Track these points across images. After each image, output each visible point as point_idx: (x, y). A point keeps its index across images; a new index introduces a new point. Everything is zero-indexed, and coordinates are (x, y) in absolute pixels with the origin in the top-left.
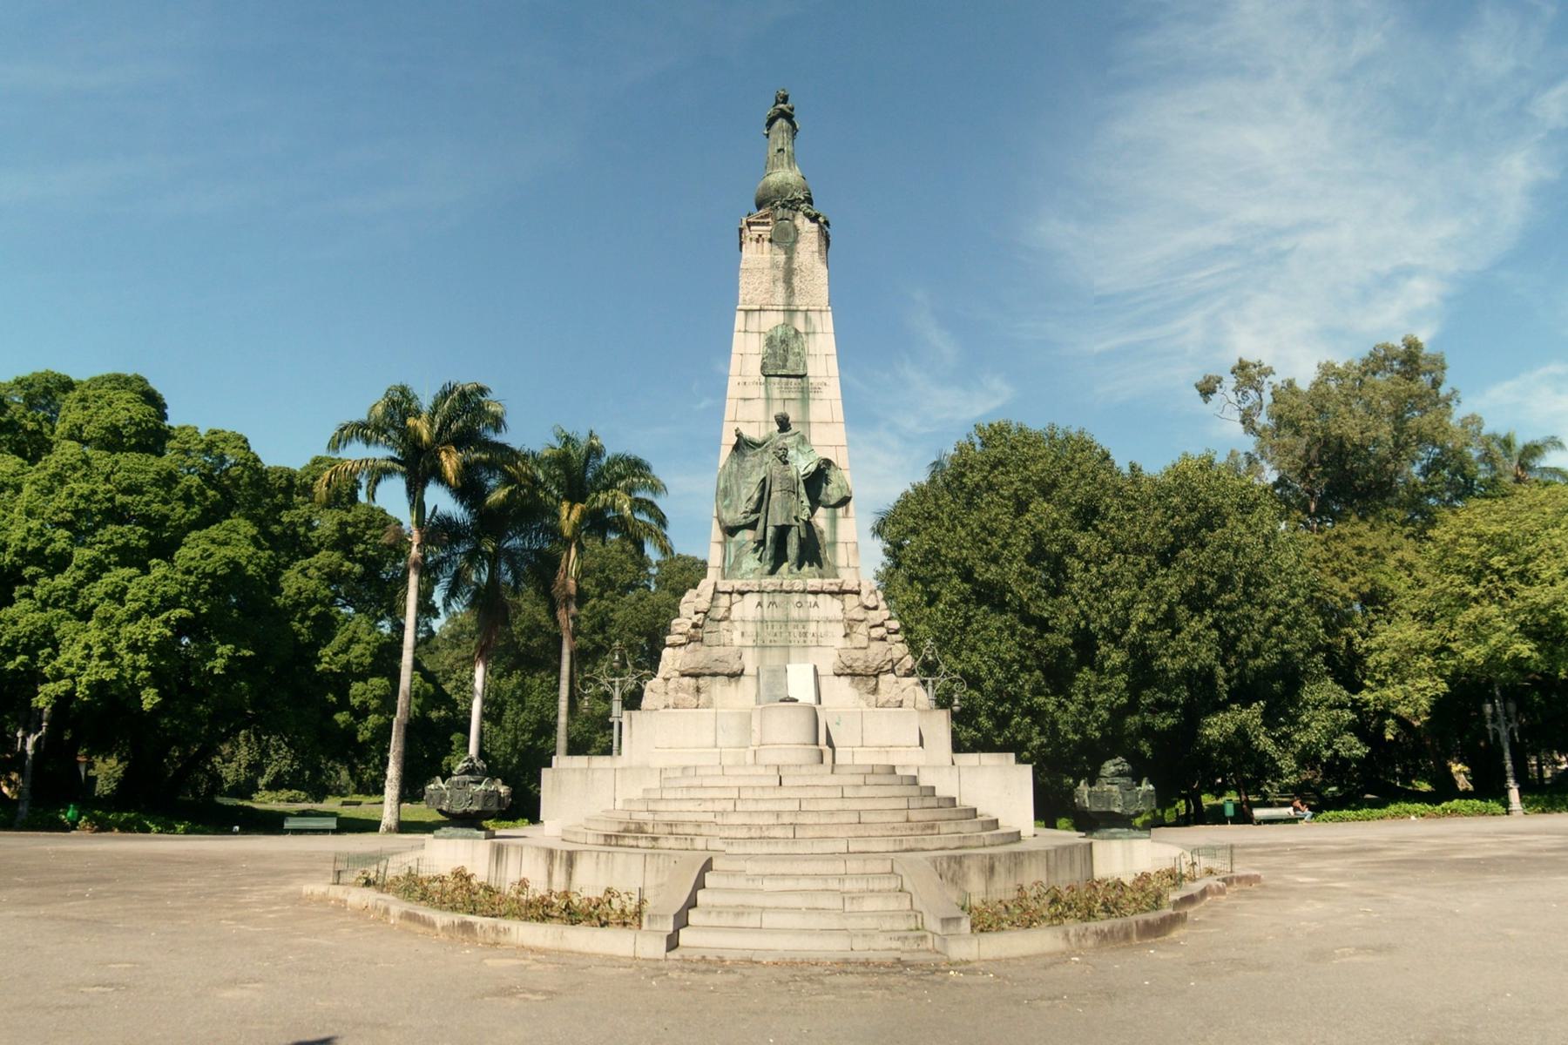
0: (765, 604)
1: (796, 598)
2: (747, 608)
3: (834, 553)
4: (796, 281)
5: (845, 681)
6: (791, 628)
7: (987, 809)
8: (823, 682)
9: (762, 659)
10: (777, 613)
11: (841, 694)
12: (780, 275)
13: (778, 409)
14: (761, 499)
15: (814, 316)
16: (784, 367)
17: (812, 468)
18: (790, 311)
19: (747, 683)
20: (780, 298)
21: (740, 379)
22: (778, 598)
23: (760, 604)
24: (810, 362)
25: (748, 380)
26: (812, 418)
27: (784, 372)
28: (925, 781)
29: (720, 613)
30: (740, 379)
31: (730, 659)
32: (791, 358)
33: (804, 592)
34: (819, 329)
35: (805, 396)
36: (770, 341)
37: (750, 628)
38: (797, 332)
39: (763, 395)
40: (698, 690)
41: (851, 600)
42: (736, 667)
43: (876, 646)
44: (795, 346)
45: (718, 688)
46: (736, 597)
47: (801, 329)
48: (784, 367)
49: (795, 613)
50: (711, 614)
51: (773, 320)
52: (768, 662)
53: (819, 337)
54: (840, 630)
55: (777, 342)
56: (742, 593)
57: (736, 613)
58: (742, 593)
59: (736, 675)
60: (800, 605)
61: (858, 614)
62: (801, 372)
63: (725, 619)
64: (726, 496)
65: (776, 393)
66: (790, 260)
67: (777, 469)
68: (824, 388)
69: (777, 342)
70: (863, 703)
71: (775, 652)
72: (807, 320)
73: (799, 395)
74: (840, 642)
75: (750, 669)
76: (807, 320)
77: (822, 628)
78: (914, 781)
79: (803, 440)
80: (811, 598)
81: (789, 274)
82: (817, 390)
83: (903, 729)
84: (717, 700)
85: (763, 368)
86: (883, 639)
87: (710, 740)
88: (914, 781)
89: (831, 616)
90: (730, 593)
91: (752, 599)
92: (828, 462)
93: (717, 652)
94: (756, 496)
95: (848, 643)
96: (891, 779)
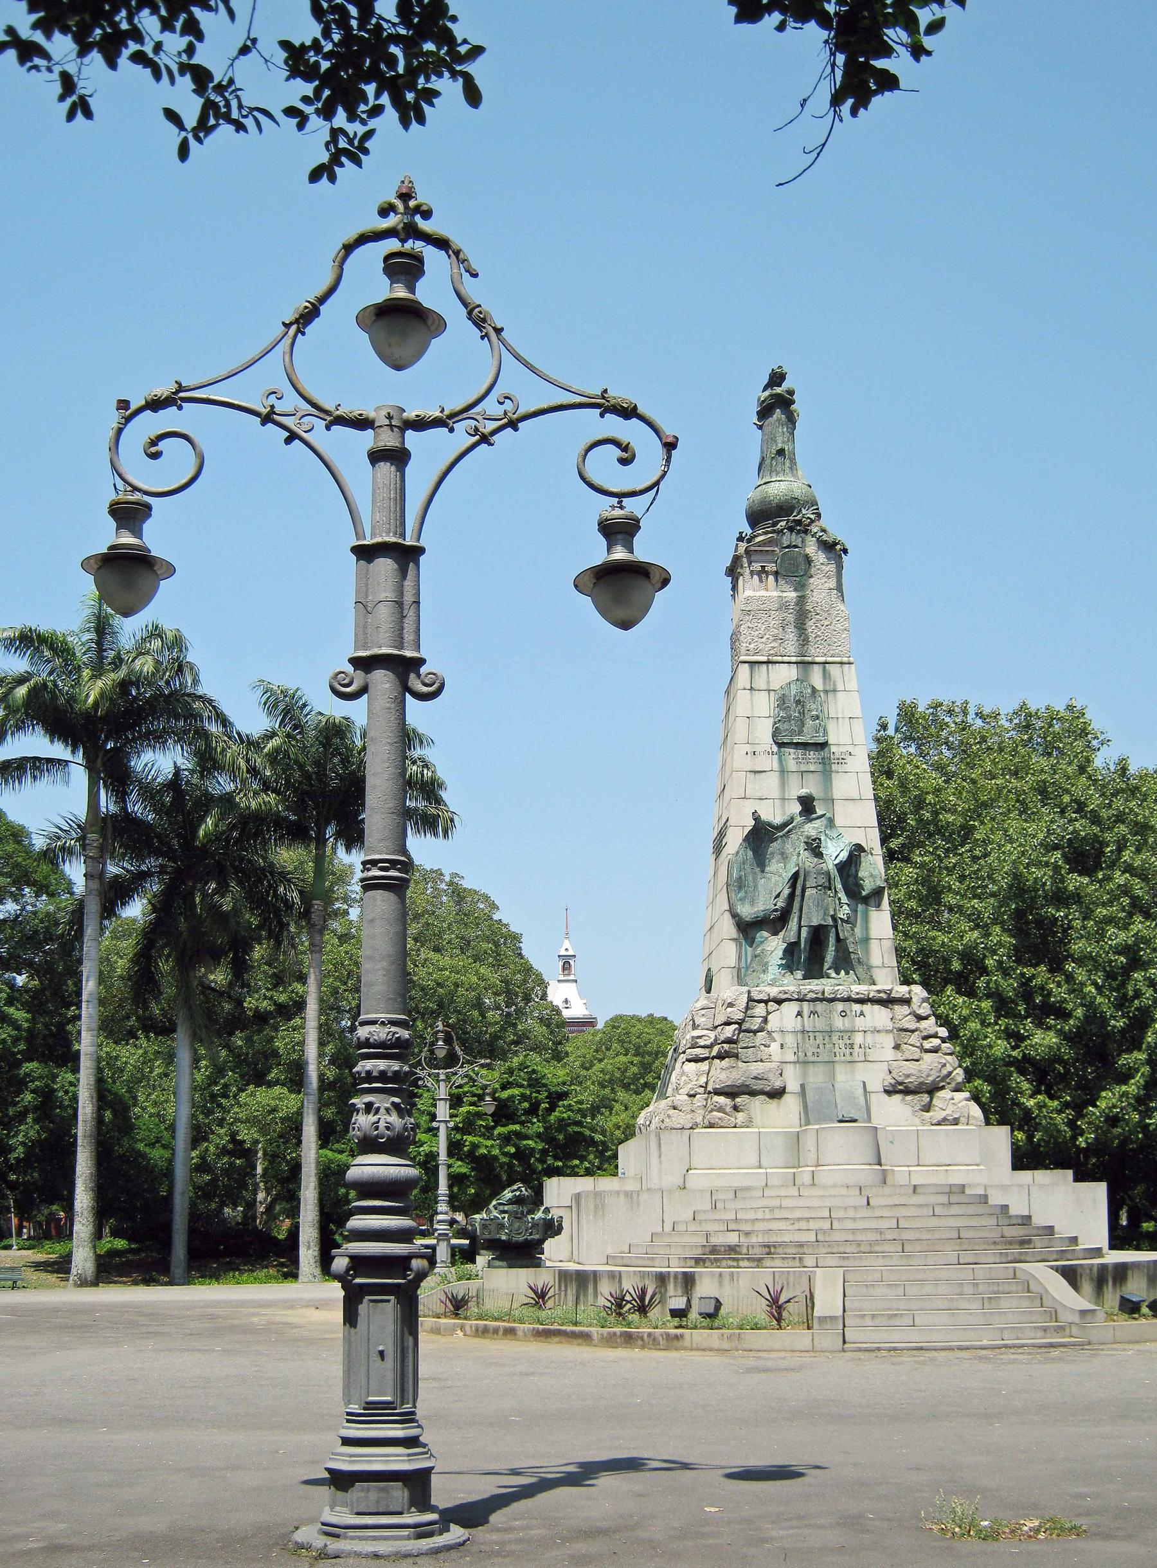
0: (806, 1013)
1: (840, 1006)
2: (785, 1018)
3: (867, 950)
4: (810, 625)
5: (897, 1098)
6: (835, 1038)
7: (1064, 1230)
8: (873, 1098)
9: (805, 1075)
10: (820, 1023)
11: (894, 1114)
12: (791, 618)
13: (797, 790)
14: (792, 896)
15: (834, 670)
16: (800, 733)
17: (844, 856)
18: (805, 665)
19: (791, 1102)
20: (791, 647)
21: (747, 748)
22: (820, 1007)
23: (799, 1014)
24: (831, 727)
25: (758, 749)
26: (836, 794)
27: (801, 739)
28: (996, 1199)
29: (755, 1024)
30: (747, 748)
31: (771, 1076)
32: (809, 723)
33: (848, 999)
34: (840, 687)
35: (826, 772)
36: (782, 702)
37: (790, 1040)
38: (814, 690)
39: (776, 766)
40: (736, 1108)
41: (901, 1010)
42: (778, 1084)
43: (928, 1057)
44: (812, 707)
45: (757, 1105)
46: (772, 1006)
47: (819, 686)
48: (800, 733)
49: (839, 1023)
50: (745, 1026)
51: (784, 675)
52: (811, 1079)
53: (839, 695)
54: (889, 1041)
55: (791, 703)
56: (779, 1002)
57: (774, 1023)
58: (779, 1002)
59: (777, 1094)
60: (843, 1014)
61: (911, 1024)
62: (821, 740)
63: (761, 1030)
64: (740, 888)
65: (792, 765)
66: (801, 600)
67: (807, 860)
68: (849, 759)
69: (791, 703)
70: (917, 1121)
71: (821, 1068)
72: (826, 675)
73: (820, 768)
74: (889, 1054)
75: (793, 1086)
76: (826, 675)
77: (870, 1038)
78: (984, 1199)
79: (831, 823)
80: (857, 1007)
81: (802, 616)
82: (841, 761)
83: (971, 1150)
84: (757, 1120)
85: (776, 733)
86: (935, 1050)
87: (753, 1160)
88: (984, 1199)
89: (879, 1026)
90: (766, 1002)
91: (790, 1009)
92: (859, 848)
93: (756, 1068)
94: (787, 892)
95: (899, 1055)
96: (980, 1209)
